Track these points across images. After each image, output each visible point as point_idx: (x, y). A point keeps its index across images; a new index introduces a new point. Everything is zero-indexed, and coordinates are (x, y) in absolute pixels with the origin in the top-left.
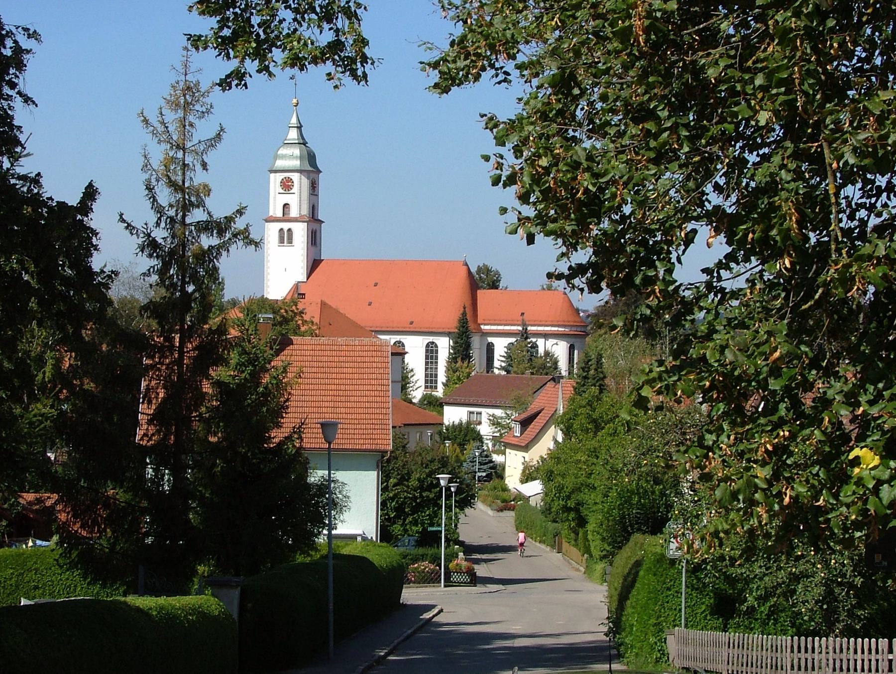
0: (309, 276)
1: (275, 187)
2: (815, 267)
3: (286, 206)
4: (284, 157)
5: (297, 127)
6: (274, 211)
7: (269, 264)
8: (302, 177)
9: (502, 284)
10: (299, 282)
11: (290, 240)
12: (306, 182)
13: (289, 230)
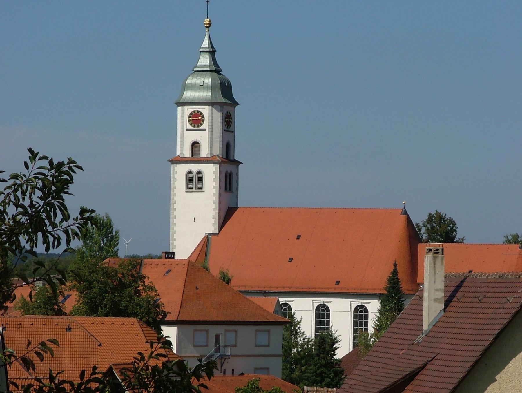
0: (222, 226)
1: (183, 123)
2: (52, 209)
3: (195, 145)
4: (193, 87)
5: (209, 52)
6: (182, 150)
7: (175, 213)
8: (214, 110)
9: (459, 236)
10: (210, 234)
11: (200, 186)
12: (218, 116)
13: (199, 173)
